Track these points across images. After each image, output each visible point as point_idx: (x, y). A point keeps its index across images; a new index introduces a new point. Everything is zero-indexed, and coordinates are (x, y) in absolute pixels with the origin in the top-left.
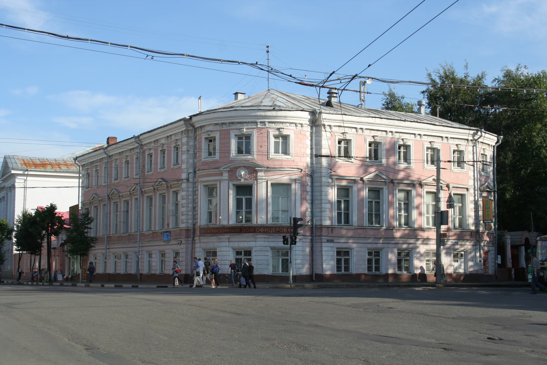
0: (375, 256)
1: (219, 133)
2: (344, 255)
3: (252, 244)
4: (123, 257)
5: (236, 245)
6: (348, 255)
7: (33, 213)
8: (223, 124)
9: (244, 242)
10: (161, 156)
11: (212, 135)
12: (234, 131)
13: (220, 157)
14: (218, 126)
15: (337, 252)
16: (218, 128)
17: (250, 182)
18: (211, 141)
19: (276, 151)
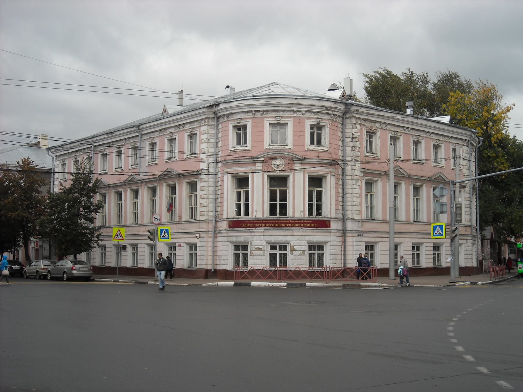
0: (280, 249)
1: (251, 121)
2: (243, 250)
3: (289, 238)
4: (129, 249)
5: (272, 239)
6: (322, 250)
7: (511, 137)
8: (256, 111)
9: (279, 236)
10: (101, 164)
11: (243, 123)
12: (270, 119)
13: (252, 147)
14: (251, 114)
15: (434, 247)
16: (250, 115)
17: (285, 173)
18: (239, 129)
19: (312, 143)
